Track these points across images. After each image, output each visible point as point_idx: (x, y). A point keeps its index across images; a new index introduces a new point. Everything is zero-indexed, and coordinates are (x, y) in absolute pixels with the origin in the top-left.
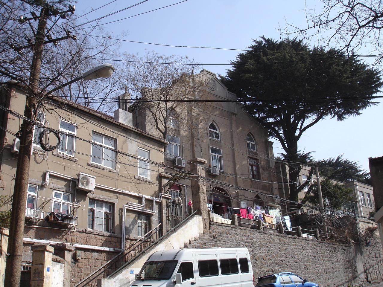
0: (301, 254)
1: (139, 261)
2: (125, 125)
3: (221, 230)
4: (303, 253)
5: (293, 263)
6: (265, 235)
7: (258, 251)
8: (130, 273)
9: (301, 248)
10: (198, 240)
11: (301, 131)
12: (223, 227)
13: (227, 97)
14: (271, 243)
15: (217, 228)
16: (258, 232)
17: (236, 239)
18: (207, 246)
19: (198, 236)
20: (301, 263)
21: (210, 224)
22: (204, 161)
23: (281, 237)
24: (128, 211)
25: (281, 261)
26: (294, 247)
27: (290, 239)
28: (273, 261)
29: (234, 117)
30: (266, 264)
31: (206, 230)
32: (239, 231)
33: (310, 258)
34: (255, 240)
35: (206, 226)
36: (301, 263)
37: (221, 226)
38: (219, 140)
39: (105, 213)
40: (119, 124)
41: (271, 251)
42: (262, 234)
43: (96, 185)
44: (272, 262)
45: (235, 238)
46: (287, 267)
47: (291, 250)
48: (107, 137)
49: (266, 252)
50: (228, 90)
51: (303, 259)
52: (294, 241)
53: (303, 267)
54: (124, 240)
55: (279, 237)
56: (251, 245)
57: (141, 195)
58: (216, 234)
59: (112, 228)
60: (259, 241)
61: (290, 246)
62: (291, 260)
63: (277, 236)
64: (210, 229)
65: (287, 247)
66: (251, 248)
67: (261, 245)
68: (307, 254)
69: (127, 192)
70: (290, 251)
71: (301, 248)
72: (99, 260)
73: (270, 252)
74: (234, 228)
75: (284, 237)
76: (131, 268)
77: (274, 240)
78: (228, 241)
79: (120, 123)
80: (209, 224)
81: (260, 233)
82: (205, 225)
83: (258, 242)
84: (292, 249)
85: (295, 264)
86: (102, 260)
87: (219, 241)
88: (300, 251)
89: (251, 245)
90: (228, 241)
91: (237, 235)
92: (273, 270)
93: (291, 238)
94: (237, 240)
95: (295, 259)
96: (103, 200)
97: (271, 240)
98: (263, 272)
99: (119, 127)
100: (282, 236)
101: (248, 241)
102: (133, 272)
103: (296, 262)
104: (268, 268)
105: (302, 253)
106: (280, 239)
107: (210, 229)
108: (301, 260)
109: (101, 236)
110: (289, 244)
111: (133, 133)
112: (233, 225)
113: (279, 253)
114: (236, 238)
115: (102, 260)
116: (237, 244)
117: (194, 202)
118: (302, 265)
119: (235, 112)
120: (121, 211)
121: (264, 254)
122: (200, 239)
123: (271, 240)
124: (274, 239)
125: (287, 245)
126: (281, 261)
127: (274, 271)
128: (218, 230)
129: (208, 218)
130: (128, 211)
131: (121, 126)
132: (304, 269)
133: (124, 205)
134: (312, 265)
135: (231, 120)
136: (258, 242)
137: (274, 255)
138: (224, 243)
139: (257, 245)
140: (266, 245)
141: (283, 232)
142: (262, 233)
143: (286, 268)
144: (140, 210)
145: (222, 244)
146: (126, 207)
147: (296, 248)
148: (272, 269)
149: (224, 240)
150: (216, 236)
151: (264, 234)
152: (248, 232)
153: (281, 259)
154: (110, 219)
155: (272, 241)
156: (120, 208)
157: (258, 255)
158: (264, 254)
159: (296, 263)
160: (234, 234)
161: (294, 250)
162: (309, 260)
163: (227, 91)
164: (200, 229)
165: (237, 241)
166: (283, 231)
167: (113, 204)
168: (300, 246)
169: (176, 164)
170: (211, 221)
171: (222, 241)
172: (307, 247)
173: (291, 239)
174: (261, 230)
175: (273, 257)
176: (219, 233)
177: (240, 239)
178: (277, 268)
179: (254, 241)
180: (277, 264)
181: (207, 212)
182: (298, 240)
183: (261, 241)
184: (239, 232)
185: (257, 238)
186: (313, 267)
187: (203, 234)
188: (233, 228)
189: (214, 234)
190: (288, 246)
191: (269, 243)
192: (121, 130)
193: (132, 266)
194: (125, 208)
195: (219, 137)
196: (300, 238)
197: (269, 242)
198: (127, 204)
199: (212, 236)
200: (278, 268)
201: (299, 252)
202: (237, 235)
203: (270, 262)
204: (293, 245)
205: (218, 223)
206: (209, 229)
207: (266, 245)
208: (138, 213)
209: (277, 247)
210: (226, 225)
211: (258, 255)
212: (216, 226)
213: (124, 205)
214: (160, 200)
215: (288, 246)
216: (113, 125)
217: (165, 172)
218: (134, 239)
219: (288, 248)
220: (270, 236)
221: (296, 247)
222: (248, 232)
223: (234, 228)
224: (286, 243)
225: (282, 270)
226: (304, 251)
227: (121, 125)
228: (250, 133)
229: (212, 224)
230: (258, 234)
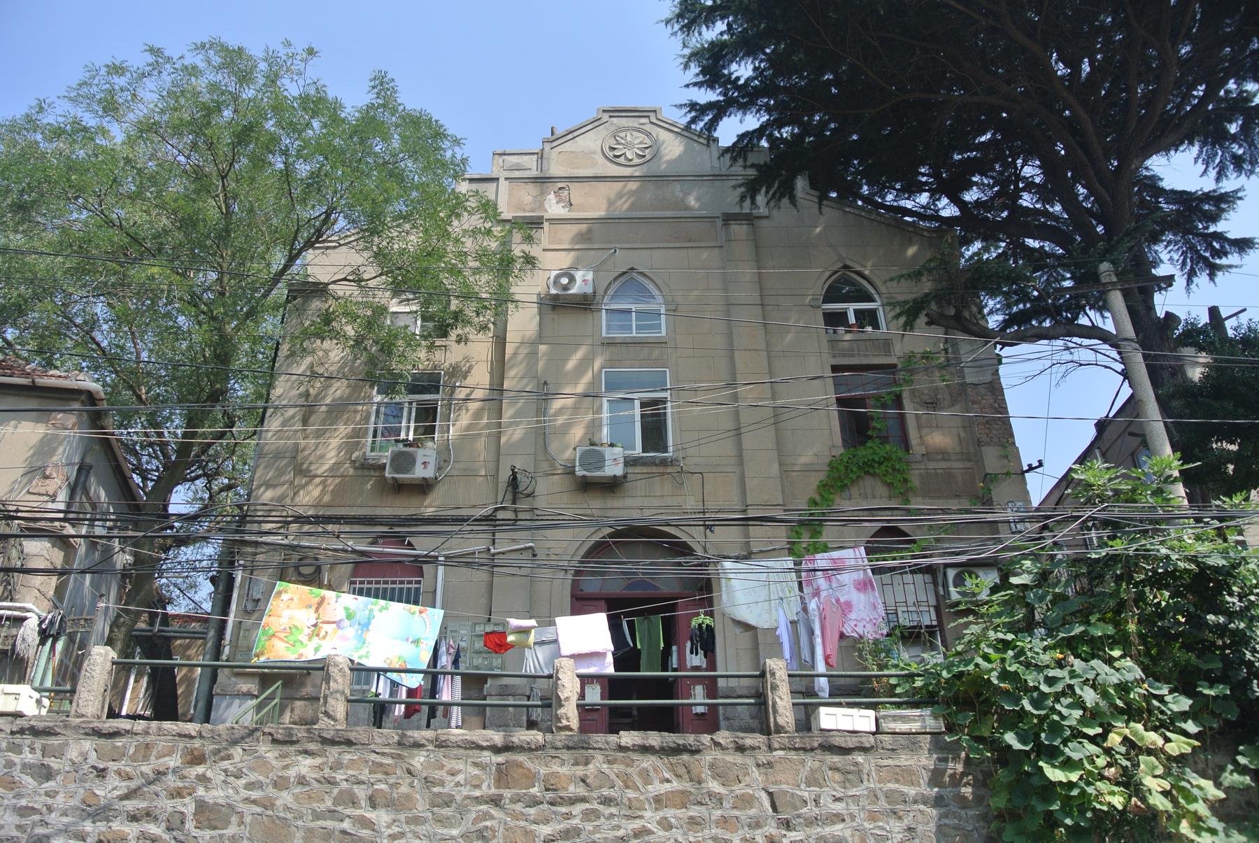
60: (254, 802)
63: (481, 748)
75: (566, 755)
110: (607, 801)
125: (578, 809)
140: (329, 824)
165: (22, 816)
215: (589, 815)
221: (694, 811)
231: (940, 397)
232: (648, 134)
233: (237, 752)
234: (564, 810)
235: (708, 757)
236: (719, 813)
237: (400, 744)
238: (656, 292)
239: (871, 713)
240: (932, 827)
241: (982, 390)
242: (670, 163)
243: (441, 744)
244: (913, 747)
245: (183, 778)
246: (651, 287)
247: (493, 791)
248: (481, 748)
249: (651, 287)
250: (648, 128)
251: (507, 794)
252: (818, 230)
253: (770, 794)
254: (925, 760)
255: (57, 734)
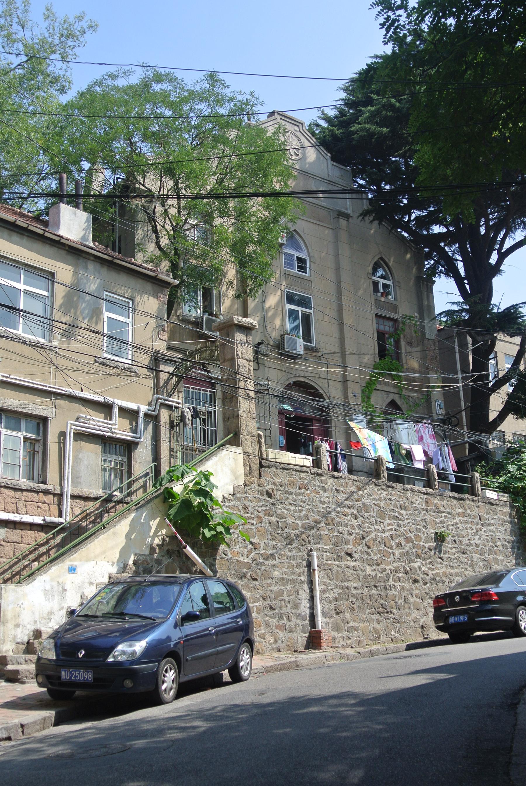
0: (475, 534)
1: (89, 546)
2: (70, 240)
3: (285, 478)
4: (482, 532)
5: (457, 555)
6: (393, 492)
7: (372, 527)
8: (67, 572)
9: (476, 520)
10: (229, 500)
11: (502, 257)
12: (291, 471)
13: (328, 175)
14: (405, 509)
15: (276, 475)
16: (375, 485)
17: (322, 499)
18: (252, 514)
19: (231, 491)
20: (475, 556)
21: (261, 466)
22: (251, 324)
23: (429, 497)
24: (80, 436)
25: (426, 550)
26: (461, 518)
27: (452, 502)
28: (407, 548)
29: (343, 222)
30: (391, 555)
31: (250, 479)
32: (331, 481)
33: (498, 543)
34: (367, 502)
35: (250, 469)
36: (475, 556)
37: (288, 469)
38: (308, 275)
39: (26, 439)
40: (57, 239)
41: (405, 526)
42: (383, 489)
43: (2, 376)
44: (404, 551)
45: (318, 496)
46: (441, 563)
47: (453, 525)
48: (29, 268)
49: (392, 529)
50: (333, 159)
51: (480, 546)
52: (463, 507)
53: (481, 563)
54: (69, 500)
55: (425, 497)
56: (358, 514)
57: (111, 400)
58: (274, 487)
59: (40, 473)
60: (376, 505)
61: (450, 516)
62: (451, 548)
63: (421, 493)
64: (260, 476)
65: (443, 518)
66: (356, 519)
67: (382, 514)
68: (491, 535)
69: (78, 393)
70: (451, 527)
71: (476, 520)
72: (9, 542)
73: (400, 529)
74: (318, 474)
75: (438, 497)
76: (71, 561)
77: (412, 503)
78: (303, 504)
79: (61, 237)
80: (258, 465)
81: (380, 488)
82: (250, 467)
83: (374, 506)
84: (456, 524)
85: (461, 556)
86: (17, 543)
87: (281, 503)
88: (474, 527)
89: (358, 514)
90: (303, 504)
91: (325, 491)
92: (408, 569)
93: (455, 498)
94: (323, 503)
95: (463, 547)
96: (20, 410)
97: (405, 503)
98: (382, 572)
99: (61, 246)
100: (433, 495)
101: (350, 503)
102: (74, 570)
103: (464, 553)
104: (396, 565)
105: (480, 532)
106: (426, 501)
107: (260, 476)
108: (476, 548)
109: (15, 489)
110: (448, 513)
111: (92, 258)
112: (315, 469)
113: (423, 533)
114: (320, 497)
115: (17, 543)
116: (323, 510)
117: (227, 415)
118: (478, 558)
119: (347, 209)
120: (62, 438)
121: (387, 534)
122: (235, 498)
123: (405, 503)
124: (414, 500)
125: (443, 515)
126: (426, 550)
127: (410, 572)
128: (279, 480)
129: (257, 453)
130: (80, 436)
131: (64, 244)
132: (481, 568)
133: (70, 422)
134: (502, 561)
135: (336, 230)
136: (374, 506)
137: (410, 535)
138: (292, 508)
139: (372, 514)
140: (393, 513)
141: (435, 485)
142: (384, 487)
143: (439, 566)
144: (130, 438)
145: (286, 509)
146: (73, 427)
147: (466, 522)
148: (404, 567)
149: (292, 502)
150: (275, 491)
151: (390, 489)
152: (350, 483)
153: (427, 545)
154: (38, 452)
155: (407, 504)
156: (61, 431)
157: (373, 535)
158: (387, 534)
159: (464, 555)
160: (317, 488)
161: (459, 525)
162: (496, 548)
163: (330, 162)
164: (236, 478)
165: (323, 504)
166: (436, 483)
167: (44, 420)
168: (475, 517)
169: (286, 347)
170: (263, 459)
171: (287, 503)
172: (492, 519)
173: (455, 502)
174: (383, 479)
175: (408, 540)
176: (281, 486)
177: (330, 500)
178: (416, 565)
179: (364, 504)
180: (418, 556)
181: (256, 439)
182: (472, 503)
183: (382, 504)
184: (329, 484)
185: (371, 498)
186: (504, 563)
187: (243, 487)
188: (314, 474)
189: (269, 487)
190: (446, 517)
191: (401, 509)
192: (65, 252)
193: (72, 557)
194: (71, 429)
195: (308, 270)
196: (475, 498)
197: (400, 506)
198: (77, 419)
199: (265, 493)
200: (419, 564)
201: (472, 530)
202: (325, 491)
203: (400, 551)
204: (459, 515)
205: (280, 463)
206: (257, 476)
207: (393, 513)
208: (102, 439)
209: (419, 519)
210: (301, 469)
211: (373, 535)
212: (274, 469)
213: (70, 422)
214: (154, 411)
215: (446, 517)
216: (44, 242)
217: (169, 348)
218: (92, 496)
219: (446, 520)
220: (404, 493)
221: (466, 518)
222: (350, 483)
223: (318, 474)
224: (442, 509)
225: (429, 569)
226: (484, 529)
227: (62, 241)
228: (382, 258)
229: (266, 467)
230: (376, 489)
231: (413, 341)
232: (299, 140)
233: (367, 487)
234: (440, 515)
235: (467, 502)
236: (470, 520)
237: (403, 489)
238: (304, 247)
239: (496, 493)
240: (509, 530)
241: (431, 342)
242: (310, 164)
243: (413, 491)
244: (506, 506)
245: (358, 495)
246: (302, 243)
247: (425, 507)
248: (421, 493)
249: (302, 243)
250: (298, 134)
251: (429, 508)
252: (372, 231)
253: (479, 516)
254: (507, 510)
255: (323, 476)
